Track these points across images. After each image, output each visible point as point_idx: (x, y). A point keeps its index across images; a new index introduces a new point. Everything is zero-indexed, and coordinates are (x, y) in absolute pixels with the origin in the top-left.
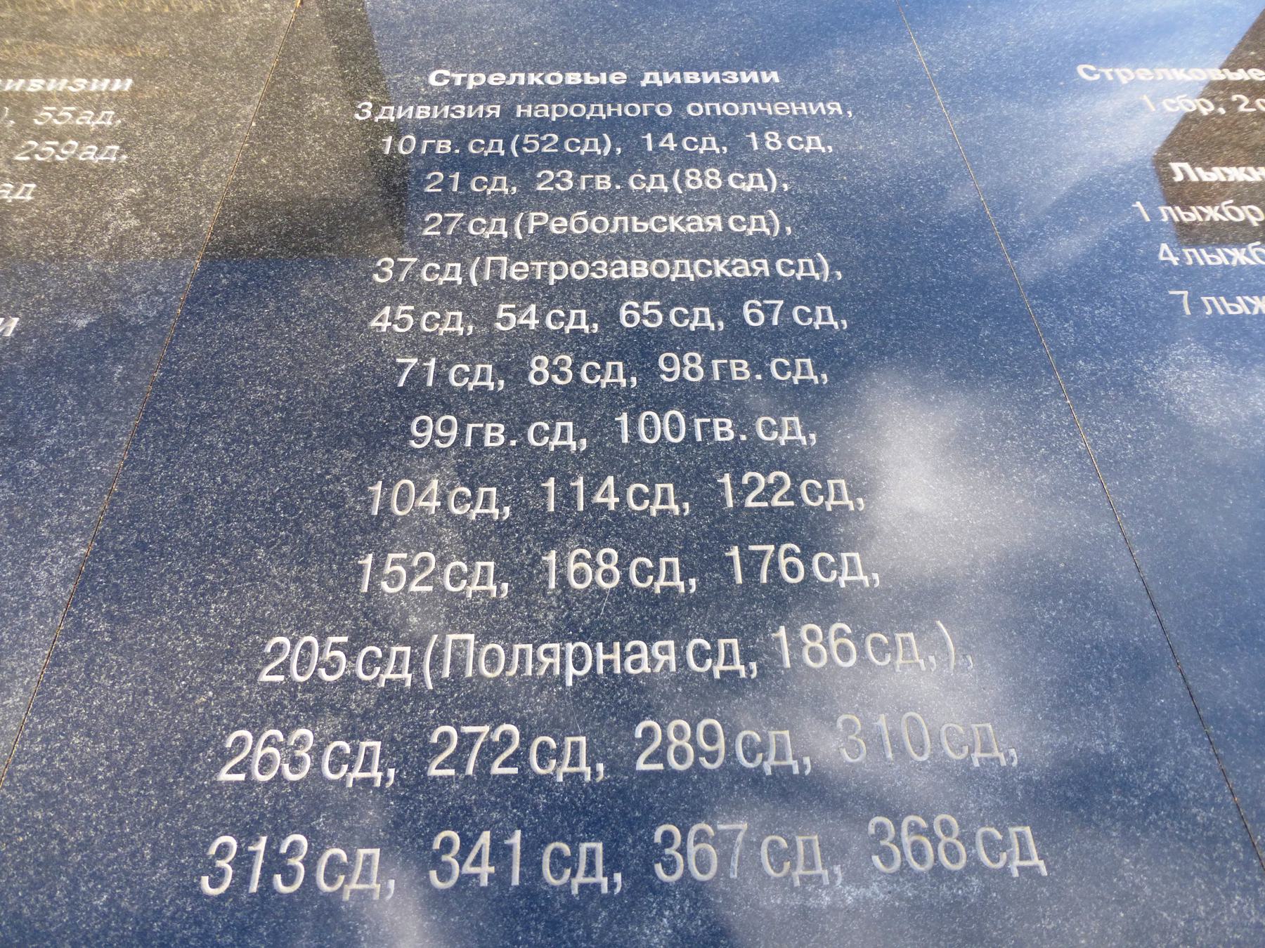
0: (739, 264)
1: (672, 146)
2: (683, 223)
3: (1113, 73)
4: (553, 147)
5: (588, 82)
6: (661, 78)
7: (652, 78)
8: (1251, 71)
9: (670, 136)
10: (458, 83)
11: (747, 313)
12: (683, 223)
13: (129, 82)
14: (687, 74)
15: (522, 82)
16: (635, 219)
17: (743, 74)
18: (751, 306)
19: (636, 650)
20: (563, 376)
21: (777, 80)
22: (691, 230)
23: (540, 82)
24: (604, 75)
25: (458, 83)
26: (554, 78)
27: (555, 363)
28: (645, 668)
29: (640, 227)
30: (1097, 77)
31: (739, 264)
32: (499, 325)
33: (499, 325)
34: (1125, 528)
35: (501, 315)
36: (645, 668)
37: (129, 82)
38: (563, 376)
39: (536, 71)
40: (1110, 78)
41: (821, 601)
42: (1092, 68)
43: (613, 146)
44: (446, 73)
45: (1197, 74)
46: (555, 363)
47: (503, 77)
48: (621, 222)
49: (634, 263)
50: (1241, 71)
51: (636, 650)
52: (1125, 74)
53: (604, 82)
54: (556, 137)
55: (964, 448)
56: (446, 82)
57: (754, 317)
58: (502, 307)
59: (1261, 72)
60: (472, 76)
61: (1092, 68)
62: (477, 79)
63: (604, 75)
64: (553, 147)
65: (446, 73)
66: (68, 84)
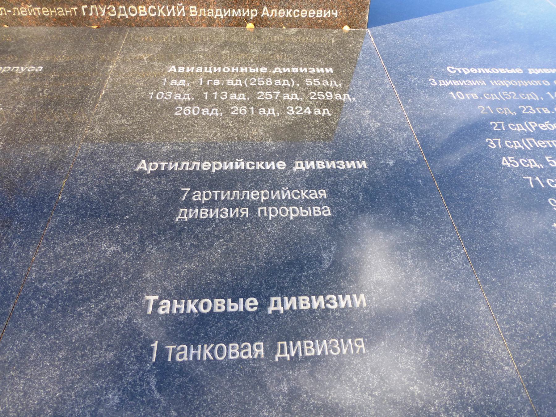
1: (310, 113)
2: (308, 194)
3: (461, 70)
4: (236, 112)
7: (277, 70)
8: (516, 69)
9: (308, 108)
12: (308, 194)
16: (230, 300)
17: (242, 68)
19: (246, 347)
21: (332, 72)
22: (312, 198)
24: (257, 68)
26: (226, 70)
28: (250, 356)
30: (455, 72)
36: (250, 356)
39: (296, 66)
40: (460, 72)
41: (342, 324)
42: (453, 68)
43: (295, 83)
45: (495, 70)
48: (246, 194)
50: (512, 69)
51: (246, 347)
52: (466, 71)
59: (554, 69)
61: (453, 68)
63: (257, 68)
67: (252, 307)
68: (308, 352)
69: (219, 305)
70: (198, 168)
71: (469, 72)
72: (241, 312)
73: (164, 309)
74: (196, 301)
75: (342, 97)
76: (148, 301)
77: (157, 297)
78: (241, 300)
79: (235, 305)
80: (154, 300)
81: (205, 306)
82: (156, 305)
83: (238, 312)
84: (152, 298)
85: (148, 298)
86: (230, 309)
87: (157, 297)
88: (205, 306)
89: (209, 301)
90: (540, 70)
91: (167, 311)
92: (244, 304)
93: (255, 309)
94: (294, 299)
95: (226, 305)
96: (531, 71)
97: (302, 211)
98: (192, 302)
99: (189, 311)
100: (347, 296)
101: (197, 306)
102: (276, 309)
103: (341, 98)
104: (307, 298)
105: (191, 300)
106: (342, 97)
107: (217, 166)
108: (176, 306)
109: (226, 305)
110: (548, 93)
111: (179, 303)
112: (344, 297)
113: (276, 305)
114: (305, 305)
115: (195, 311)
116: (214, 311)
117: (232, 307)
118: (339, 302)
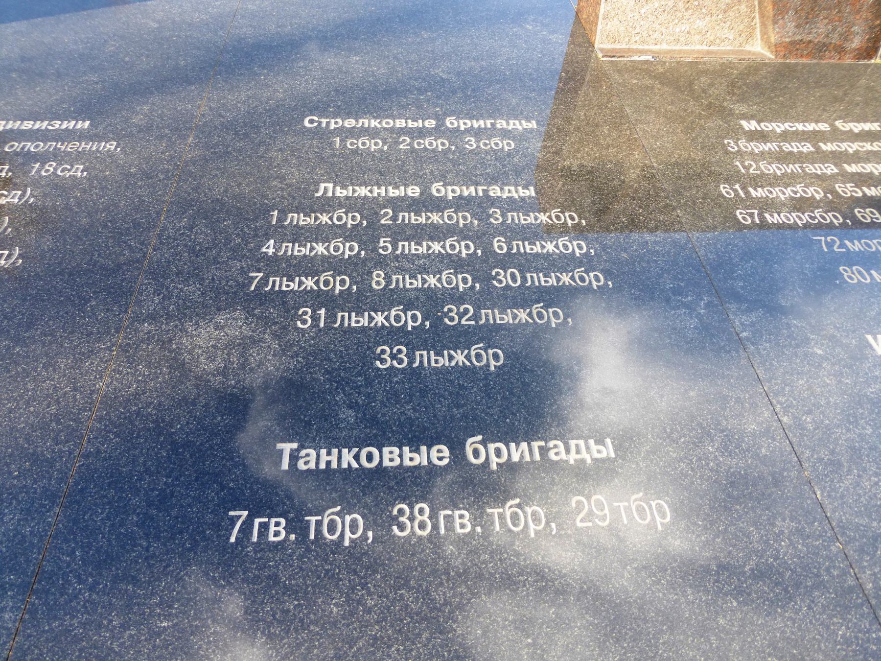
0: (555, 446)
5: (410, 125)
6: (521, 124)
8: (820, 124)
10: (324, 125)
11: (496, 245)
13: (87, 123)
14: (397, 121)
15: (366, 125)
18: (498, 241)
20: (401, 361)
23: (379, 126)
25: (324, 125)
27: (395, 351)
29: (416, 250)
31: (555, 446)
32: (381, 251)
33: (381, 251)
34: (791, 435)
35: (382, 244)
37: (87, 123)
38: (401, 361)
44: (316, 118)
45: (767, 127)
46: (395, 351)
47: (353, 121)
49: (386, 450)
52: (779, 127)
53: (421, 126)
54: (408, 140)
55: (645, 349)
56: (315, 124)
57: (501, 248)
58: (382, 240)
60: (333, 121)
62: (336, 123)
64: (407, 145)
65: (316, 118)
66: (49, 124)
67: (440, 459)
68: (260, 523)
69: (391, 456)
70: (330, 194)
71: (783, 129)
72: (424, 467)
73: (306, 463)
74: (356, 450)
75: (508, 124)
76: (281, 451)
77: (295, 445)
78: (424, 449)
79: (415, 455)
80: (291, 450)
81: (370, 457)
82: (294, 457)
83: (418, 467)
84: (287, 447)
85: (280, 446)
86: (407, 463)
87: (295, 445)
88: (370, 457)
89: (375, 451)
90: (813, 125)
91: (312, 465)
92: (428, 453)
93: (446, 461)
94: (524, 445)
95: (401, 456)
96: (437, 189)
97: (498, 316)
98: (349, 452)
99: (345, 465)
100: (404, 448)
101: (357, 457)
102: (579, 457)
103: (505, 126)
104: (396, 450)
105: (347, 450)
106: (508, 124)
107: (453, 191)
108: (324, 458)
109: (401, 456)
110: (738, 163)
111: (329, 453)
112: (518, 445)
113: (578, 452)
114: (391, 460)
115: (355, 465)
116: (384, 465)
117: (411, 459)
118: (557, 451)
